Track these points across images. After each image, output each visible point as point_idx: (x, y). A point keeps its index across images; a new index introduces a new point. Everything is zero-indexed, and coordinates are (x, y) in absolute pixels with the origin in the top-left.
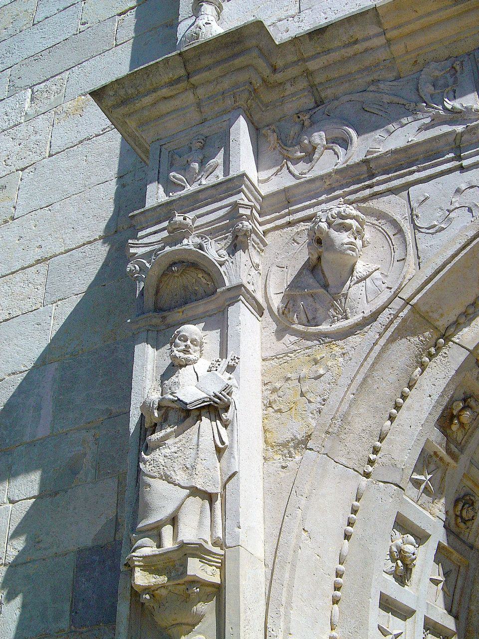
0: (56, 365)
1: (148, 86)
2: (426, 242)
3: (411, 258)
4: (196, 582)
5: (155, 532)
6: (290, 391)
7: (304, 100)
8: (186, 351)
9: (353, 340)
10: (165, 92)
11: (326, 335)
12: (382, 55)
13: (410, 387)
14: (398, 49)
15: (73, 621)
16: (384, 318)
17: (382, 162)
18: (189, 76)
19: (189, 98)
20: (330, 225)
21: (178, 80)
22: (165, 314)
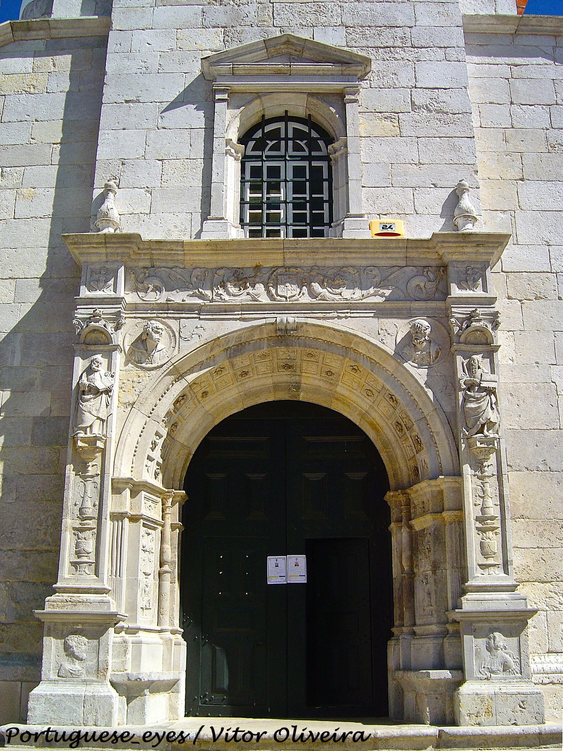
0: (21, 334)
1: (88, 241)
2: (183, 343)
3: (177, 348)
4: (98, 447)
5: (84, 429)
6: (129, 385)
7: (147, 263)
8: (98, 367)
9: (153, 372)
10: (95, 246)
11: (144, 368)
12: (180, 258)
13: (167, 391)
14: (188, 258)
15: (32, 443)
16: (164, 368)
17: (173, 305)
18: (105, 243)
19: (103, 251)
20: (152, 330)
21: (101, 243)
22: (88, 346)
